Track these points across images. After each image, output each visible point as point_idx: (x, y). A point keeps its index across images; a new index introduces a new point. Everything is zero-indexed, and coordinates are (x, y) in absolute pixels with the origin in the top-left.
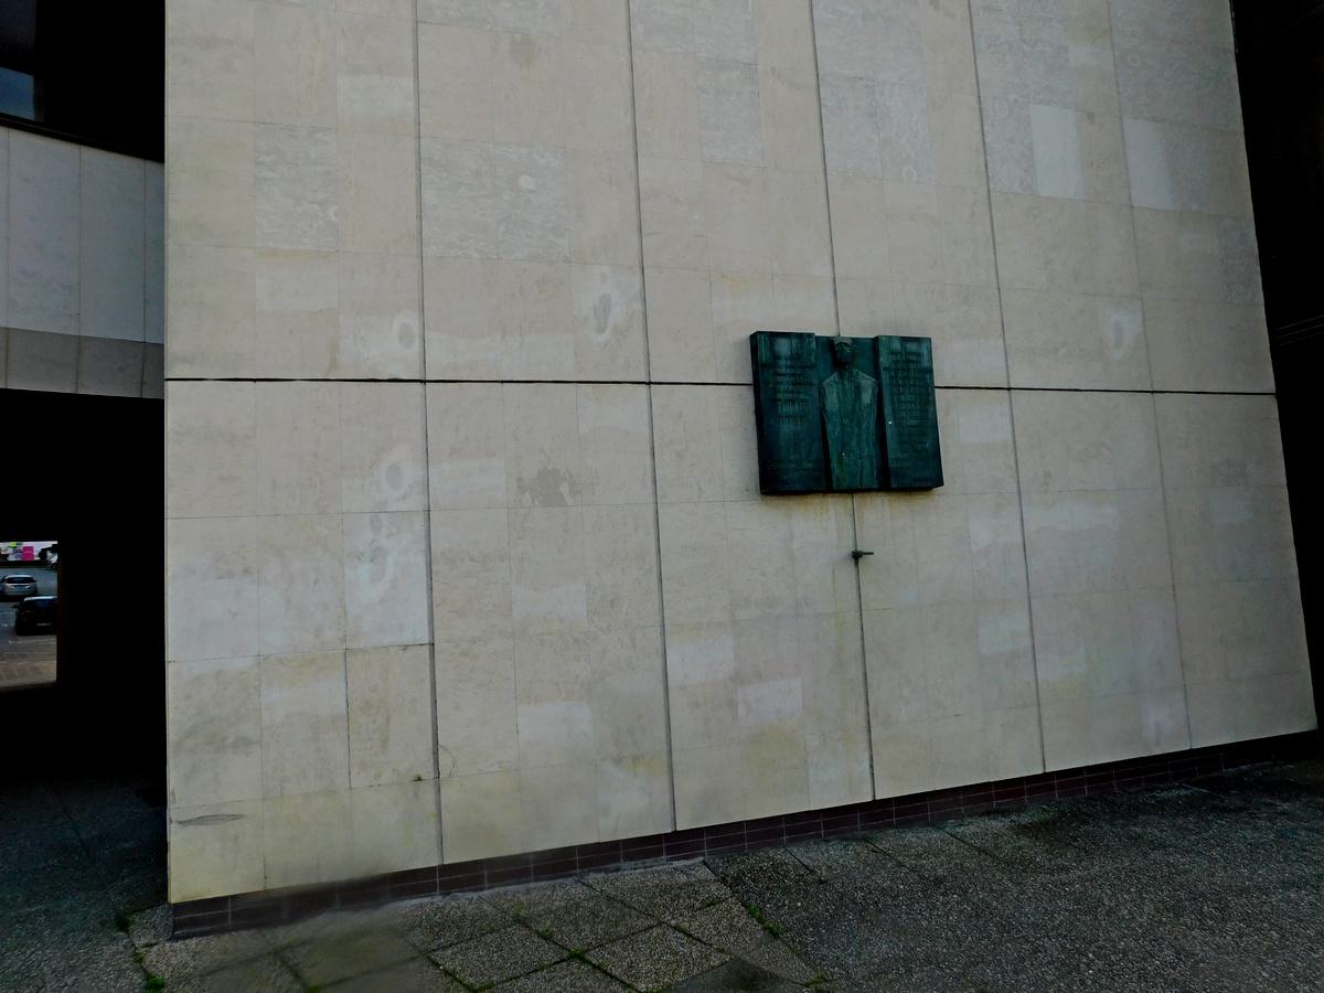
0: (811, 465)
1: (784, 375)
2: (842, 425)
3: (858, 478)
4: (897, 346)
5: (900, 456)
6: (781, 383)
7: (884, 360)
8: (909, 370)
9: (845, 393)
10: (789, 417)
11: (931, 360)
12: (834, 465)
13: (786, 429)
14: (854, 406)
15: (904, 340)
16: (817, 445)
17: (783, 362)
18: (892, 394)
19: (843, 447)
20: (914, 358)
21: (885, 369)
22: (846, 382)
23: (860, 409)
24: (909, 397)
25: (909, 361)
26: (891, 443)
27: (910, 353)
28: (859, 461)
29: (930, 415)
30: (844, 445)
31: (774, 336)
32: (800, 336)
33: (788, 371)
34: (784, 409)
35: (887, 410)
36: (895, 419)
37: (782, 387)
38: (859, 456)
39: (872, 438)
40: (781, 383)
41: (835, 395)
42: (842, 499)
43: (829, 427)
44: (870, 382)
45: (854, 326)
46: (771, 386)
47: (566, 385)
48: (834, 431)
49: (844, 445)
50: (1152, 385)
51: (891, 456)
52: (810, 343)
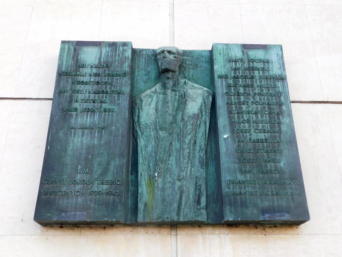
0: (105, 187)
1: (86, 83)
2: (157, 139)
3: (175, 205)
4: (238, 54)
5: (240, 177)
6: (78, 92)
7: (220, 68)
8: (252, 78)
9: (165, 102)
10: (83, 128)
11: (283, 66)
12: (143, 188)
13: (78, 142)
14: (175, 117)
15: (245, 47)
16: (118, 163)
17: (87, 70)
18: (229, 104)
19: (156, 165)
20: (260, 65)
21: (220, 77)
22: (169, 92)
23: (183, 119)
24: (253, 108)
25: (253, 69)
26: (227, 160)
27: (253, 61)
28: (178, 184)
29: (284, 128)
30: (157, 162)
31: (81, 44)
32: (113, 45)
33: (93, 79)
34: (79, 120)
35: (222, 121)
36: (232, 131)
37: (80, 96)
38: (173, 173)
39: (199, 154)
40: (78, 92)
41: (153, 105)
42: (158, 236)
43: (141, 142)
44: (200, 91)
45: (191, 36)
46: (67, 94)
47: (13, 101)
48: (146, 146)
49: (157, 162)
50: (172, 34)
51: (226, 177)
52: (124, 51)
